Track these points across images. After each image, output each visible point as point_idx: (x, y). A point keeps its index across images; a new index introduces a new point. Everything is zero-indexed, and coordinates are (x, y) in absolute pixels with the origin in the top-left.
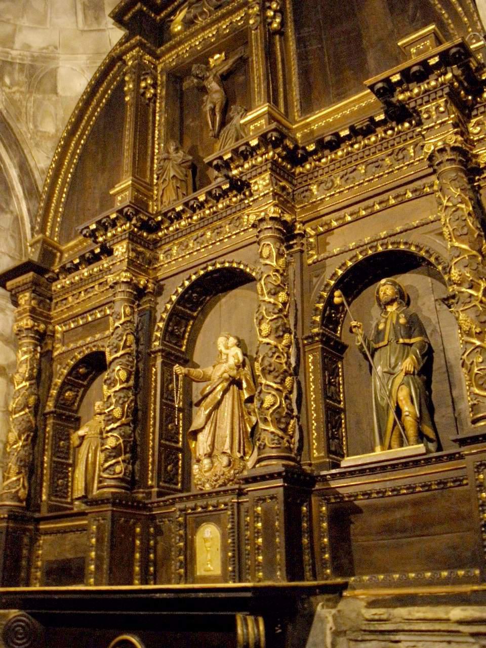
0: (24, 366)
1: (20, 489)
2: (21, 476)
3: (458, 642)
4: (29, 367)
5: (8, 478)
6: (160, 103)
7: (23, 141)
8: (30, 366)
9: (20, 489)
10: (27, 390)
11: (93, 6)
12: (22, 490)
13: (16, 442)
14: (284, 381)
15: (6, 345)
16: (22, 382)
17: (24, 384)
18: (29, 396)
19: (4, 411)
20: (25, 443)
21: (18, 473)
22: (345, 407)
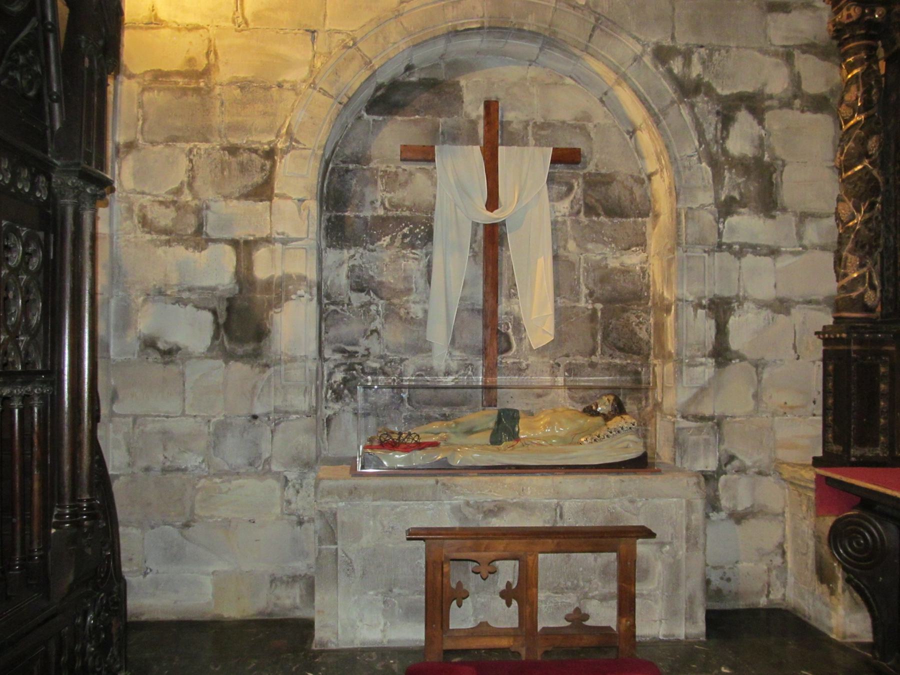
0: (853, 88)
1: (865, 291)
2: (865, 269)
3: (427, 4)
4: (861, 90)
5: (846, 275)
6: (626, 380)
7: (137, 617)
8: (864, 86)
9: (865, 291)
10: (861, 129)
11: (824, 1)
12: (870, 293)
13: (853, 217)
14: (165, 525)
15: (824, 60)
16: (852, 117)
17: (857, 118)
18: (868, 137)
19: (832, 168)
20: (867, 216)
21: (862, 266)
22: (292, 420)
